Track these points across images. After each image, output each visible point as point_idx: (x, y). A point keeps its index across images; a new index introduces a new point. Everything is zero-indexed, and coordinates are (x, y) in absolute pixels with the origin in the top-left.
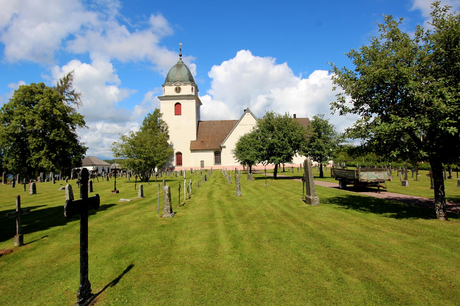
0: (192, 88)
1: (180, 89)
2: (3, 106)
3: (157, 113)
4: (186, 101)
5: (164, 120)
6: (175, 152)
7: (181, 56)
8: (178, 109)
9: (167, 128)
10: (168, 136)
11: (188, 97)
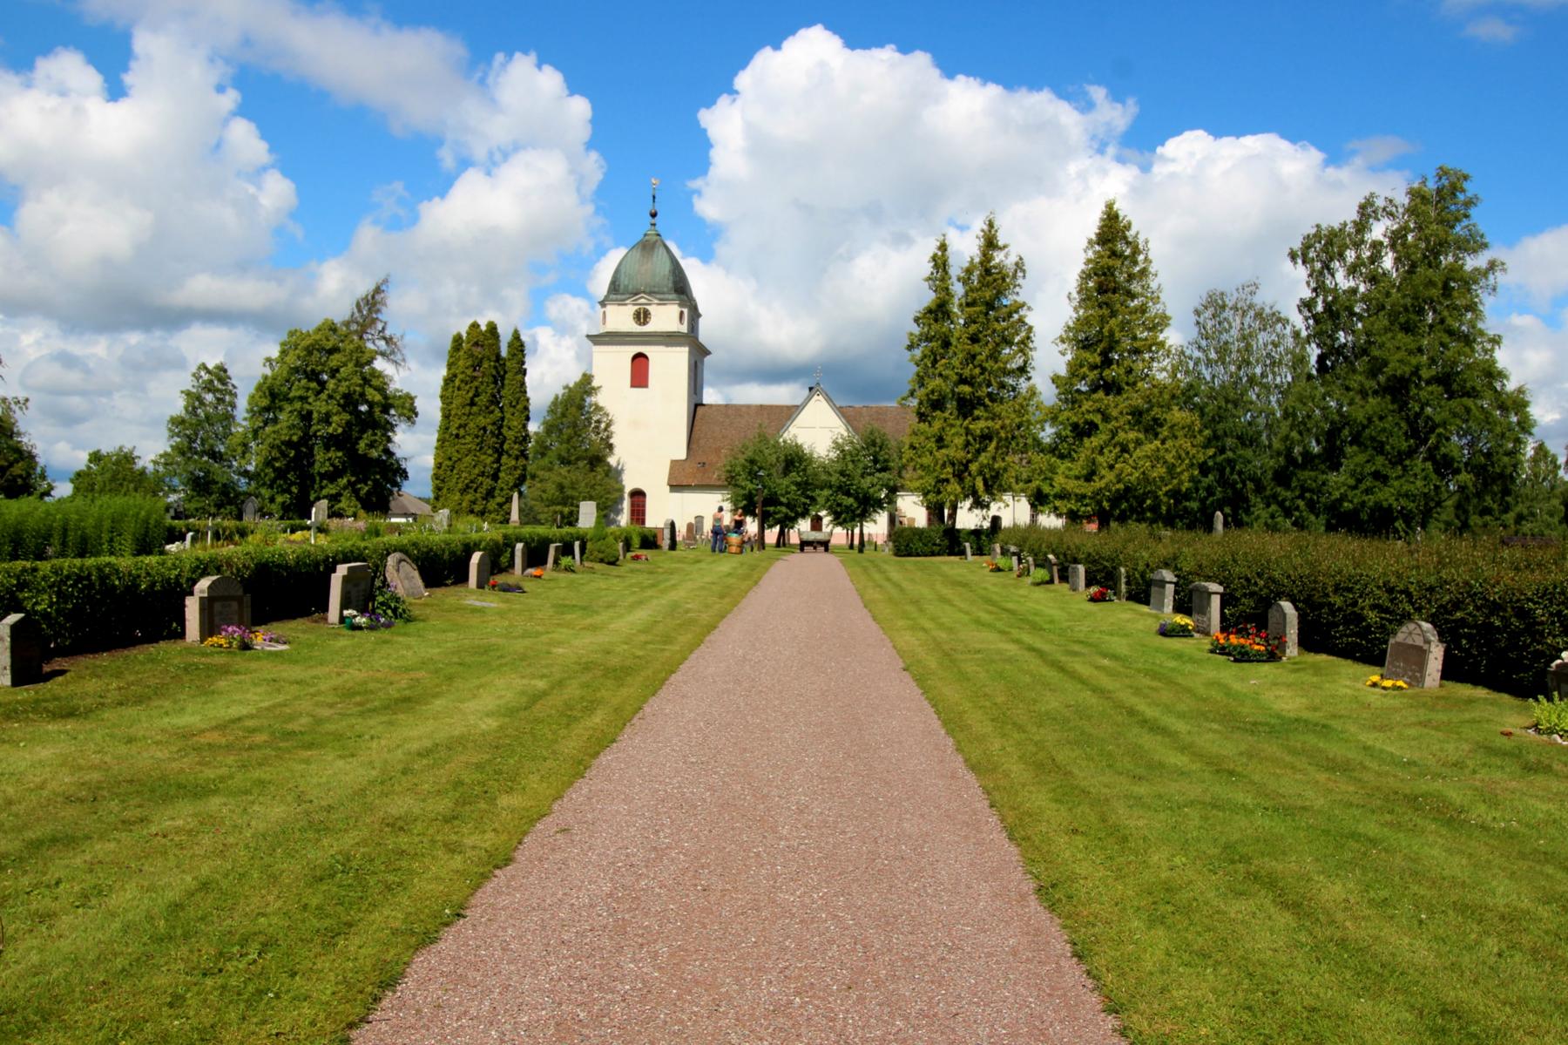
0: (682, 313)
1: (647, 314)
2: (229, 373)
3: (585, 386)
4: (662, 348)
5: (601, 404)
6: (627, 490)
7: (654, 215)
8: (640, 373)
9: (608, 425)
10: (611, 447)
11: (669, 339)
